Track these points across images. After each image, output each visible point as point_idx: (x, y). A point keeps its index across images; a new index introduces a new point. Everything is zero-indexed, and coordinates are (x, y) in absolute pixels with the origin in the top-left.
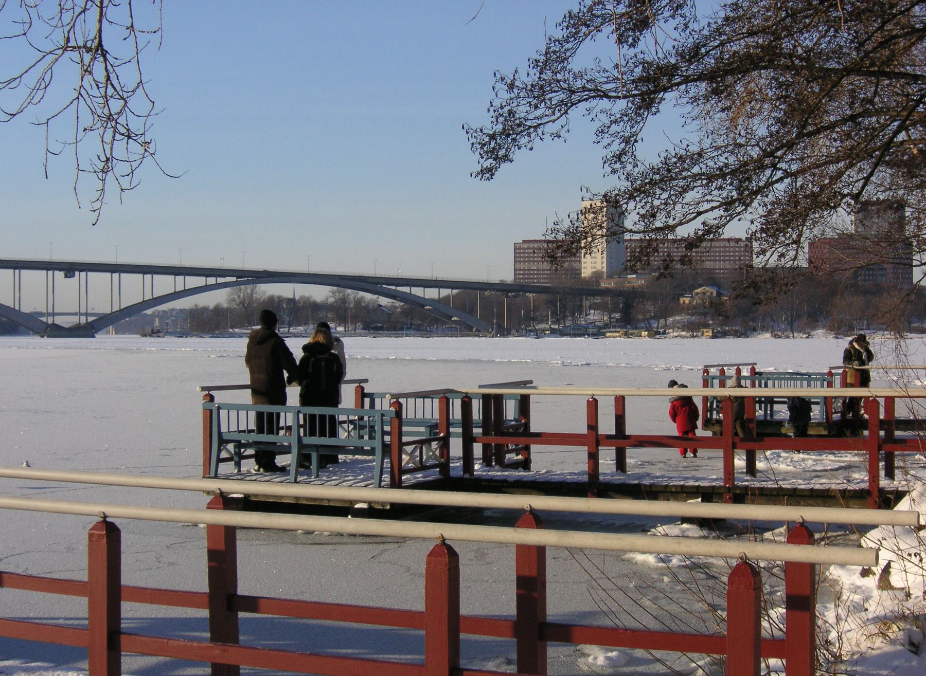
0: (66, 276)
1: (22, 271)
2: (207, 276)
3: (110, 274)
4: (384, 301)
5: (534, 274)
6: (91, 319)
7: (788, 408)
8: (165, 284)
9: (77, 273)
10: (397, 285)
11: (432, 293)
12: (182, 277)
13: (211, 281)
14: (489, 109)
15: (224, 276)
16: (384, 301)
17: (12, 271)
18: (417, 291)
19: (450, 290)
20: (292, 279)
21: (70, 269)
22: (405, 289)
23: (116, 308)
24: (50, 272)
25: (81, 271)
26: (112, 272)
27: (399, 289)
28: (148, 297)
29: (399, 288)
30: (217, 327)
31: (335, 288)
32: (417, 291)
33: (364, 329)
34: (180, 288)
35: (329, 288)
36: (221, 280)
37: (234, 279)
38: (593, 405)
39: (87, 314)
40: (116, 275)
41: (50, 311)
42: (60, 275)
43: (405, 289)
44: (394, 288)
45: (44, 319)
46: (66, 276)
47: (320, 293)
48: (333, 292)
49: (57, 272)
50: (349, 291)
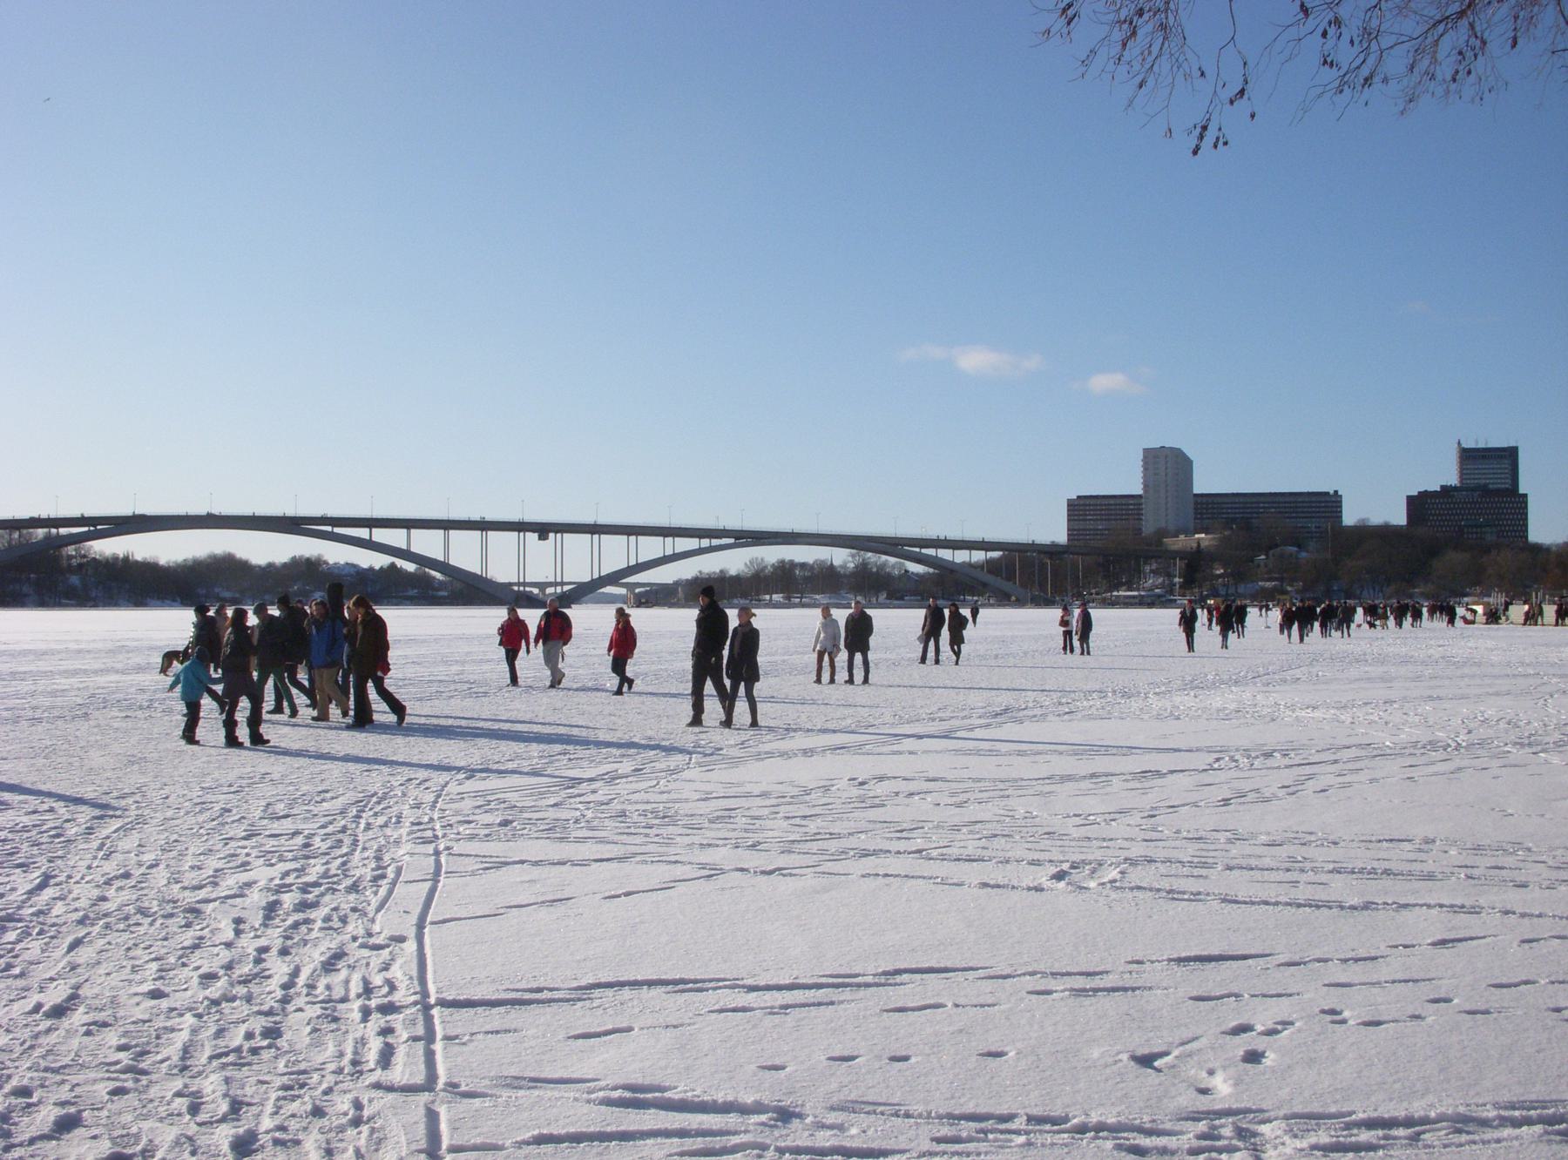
0: (540, 539)
1: (565, 535)
2: (700, 537)
3: (590, 536)
4: (915, 568)
5: (1089, 510)
6: (566, 588)
7: (565, 644)
8: (651, 547)
9: (551, 535)
10: (921, 547)
11: (961, 556)
12: (671, 539)
13: (705, 543)
14: (854, 779)
15: (720, 538)
16: (915, 568)
17: (480, 532)
18: (946, 554)
19: (696, 540)
20: (799, 540)
21: (543, 530)
22: (931, 552)
23: (596, 576)
24: (596, 537)
25: (556, 532)
26: (629, 534)
27: (924, 551)
28: (633, 562)
29: (924, 551)
30: (656, 592)
31: (854, 551)
32: (946, 554)
33: (887, 598)
34: (669, 552)
35: (848, 551)
36: (715, 542)
37: (732, 541)
38: (1349, 635)
39: (562, 584)
40: (633, 538)
41: (559, 580)
42: (532, 537)
43: (931, 552)
44: (917, 550)
45: (516, 588)
46: (540, 539)
47: (840, 557)
48: (853, 556)
49: (529, 534)
50: (870, 554)
